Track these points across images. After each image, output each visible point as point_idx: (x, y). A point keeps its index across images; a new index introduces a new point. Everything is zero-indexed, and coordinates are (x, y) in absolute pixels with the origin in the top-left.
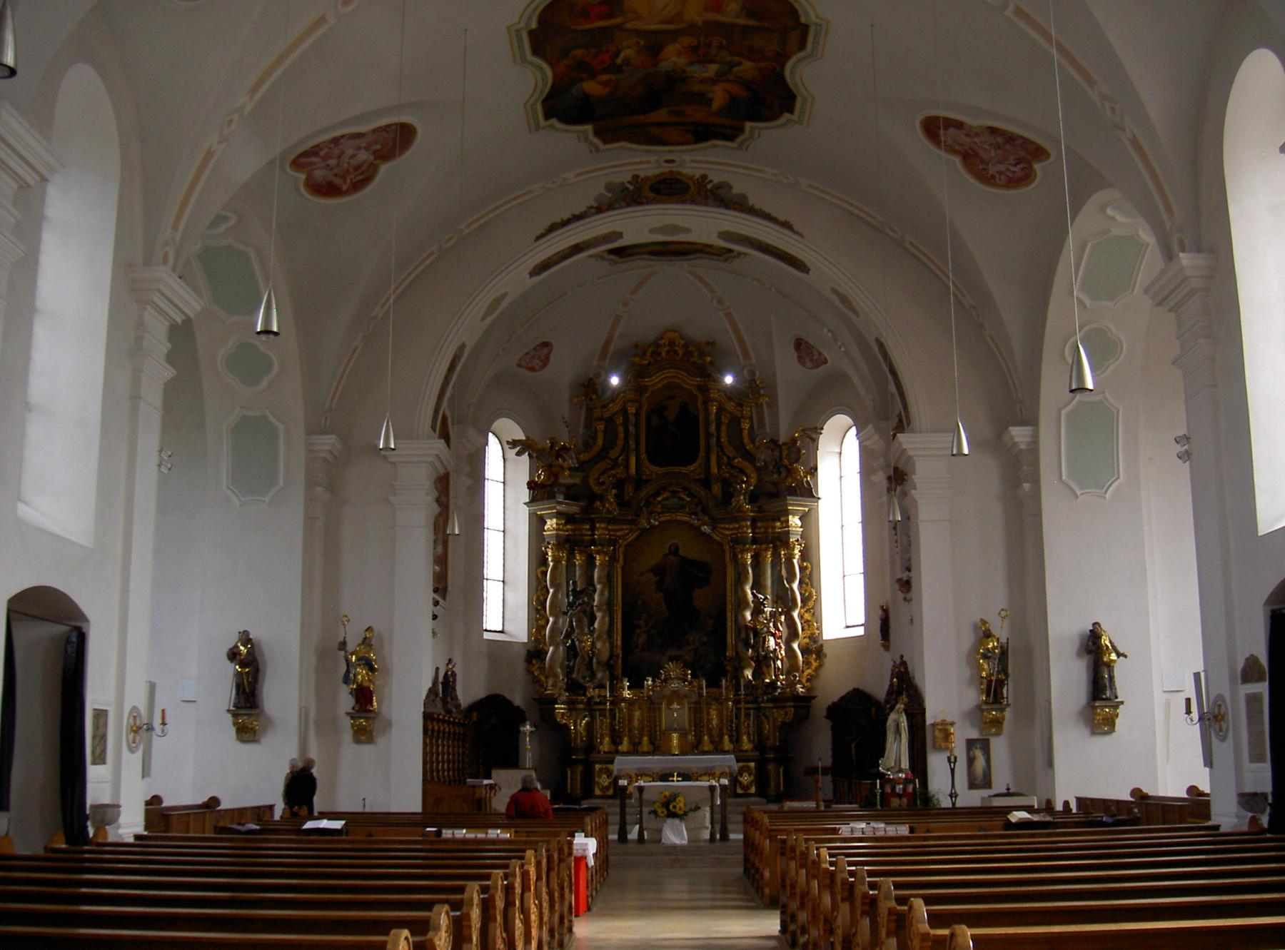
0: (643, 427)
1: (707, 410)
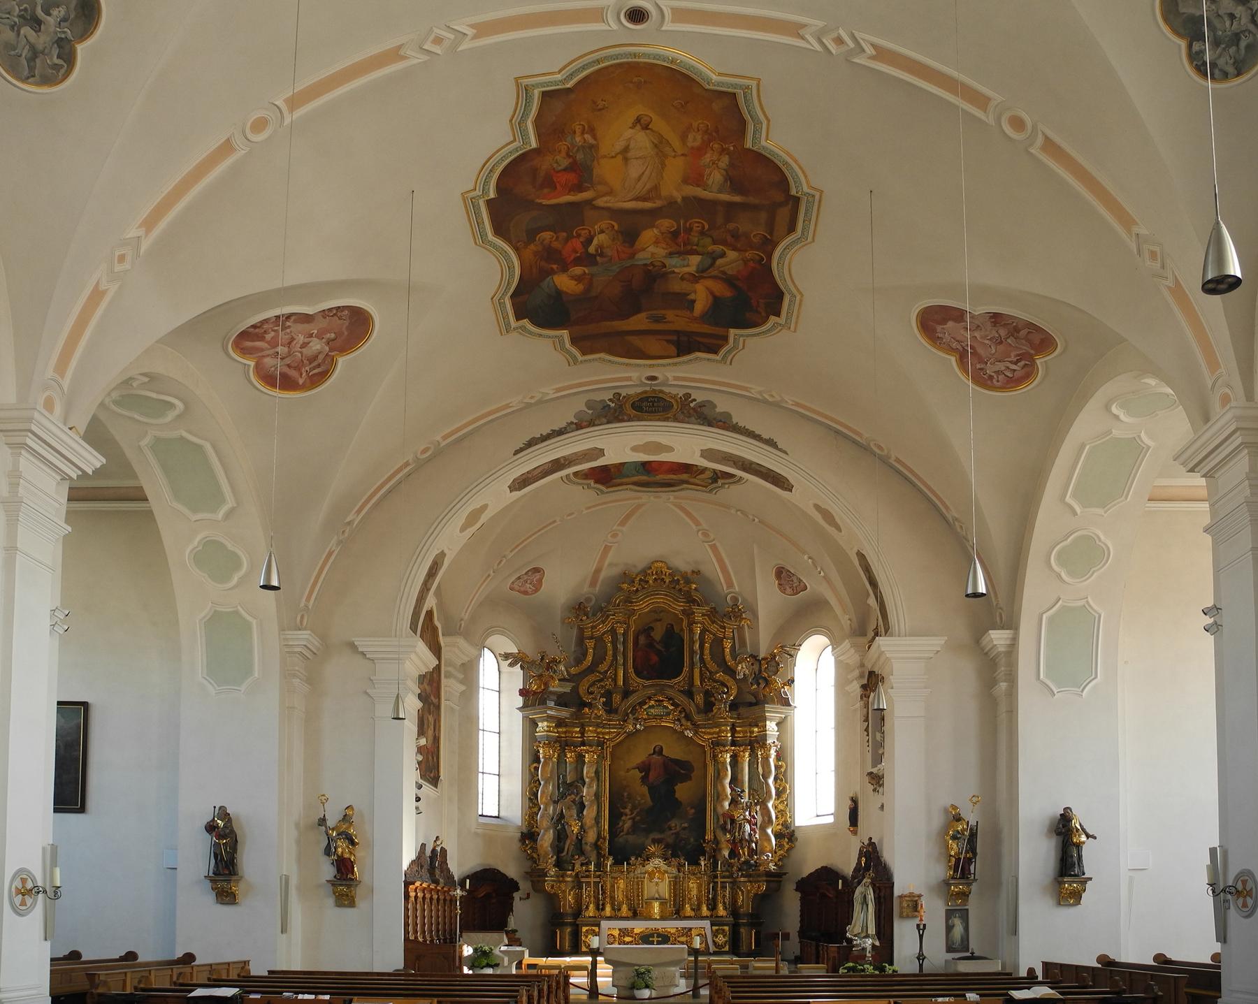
0: (631, 645)
1: (691, 631)
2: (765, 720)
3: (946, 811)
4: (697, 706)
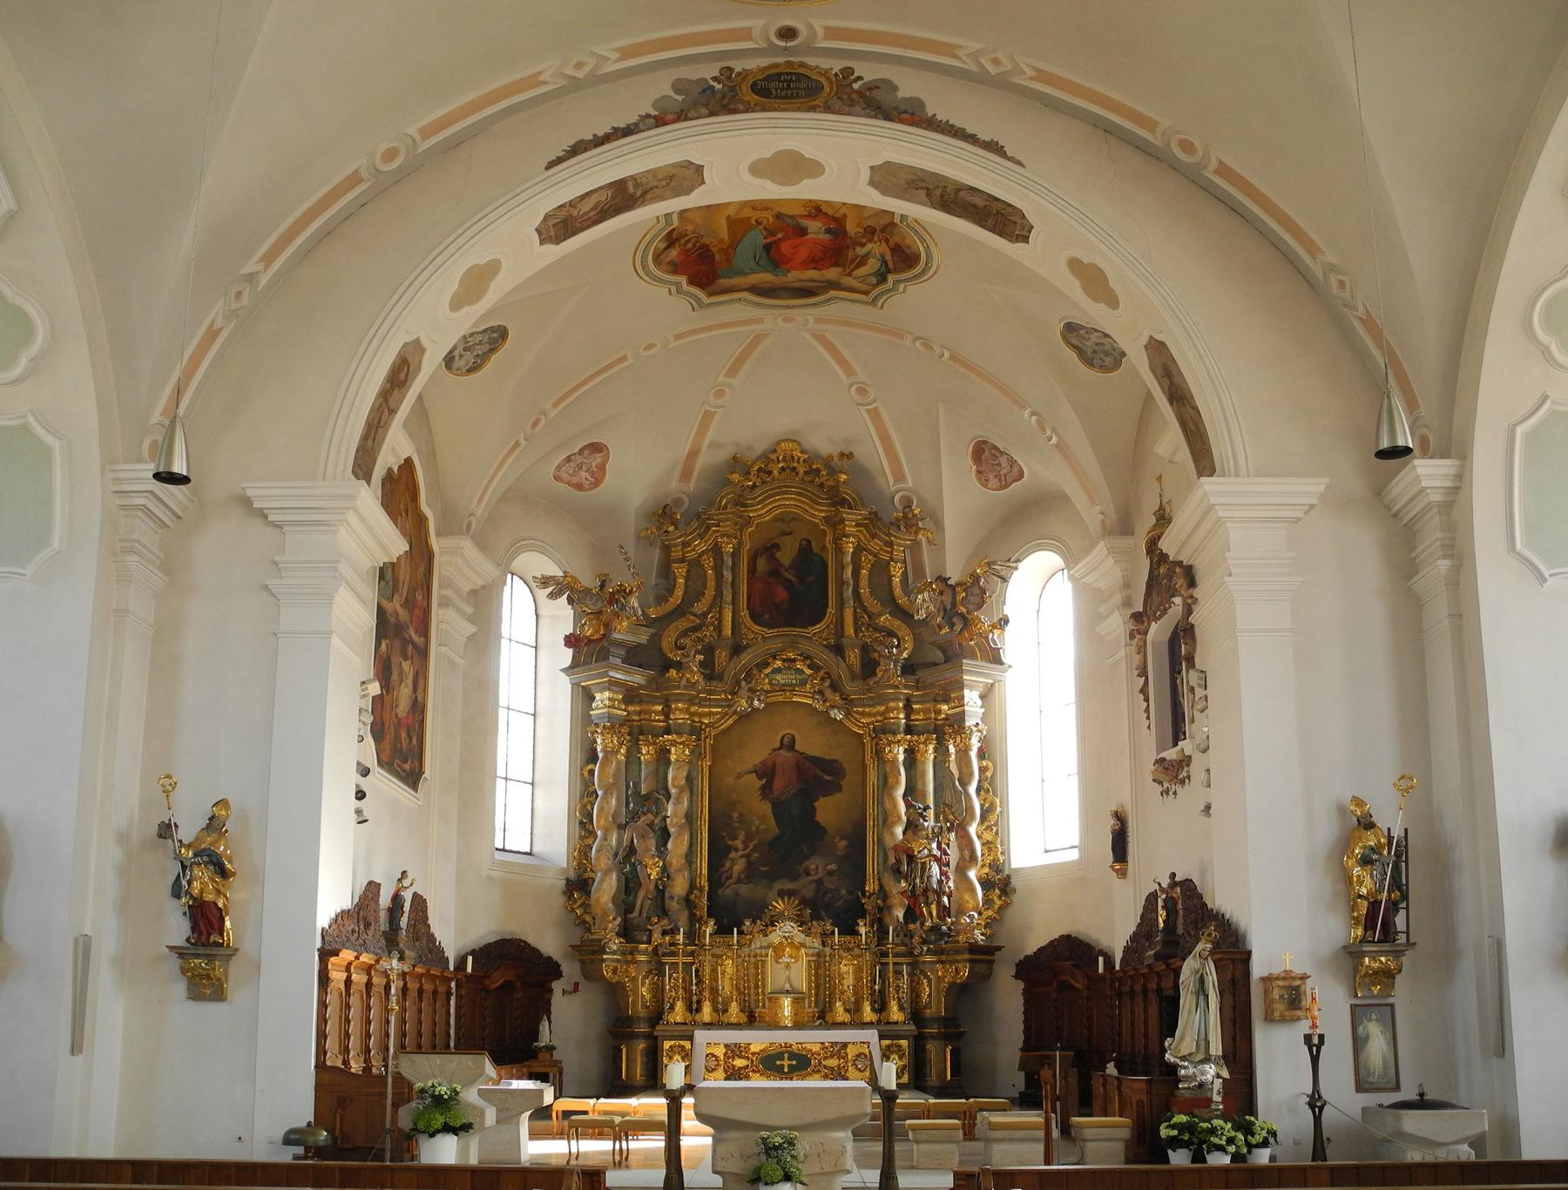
1: (839, 550)
2: (961, 688)
3: (1342, 811)
4: (850, 668)
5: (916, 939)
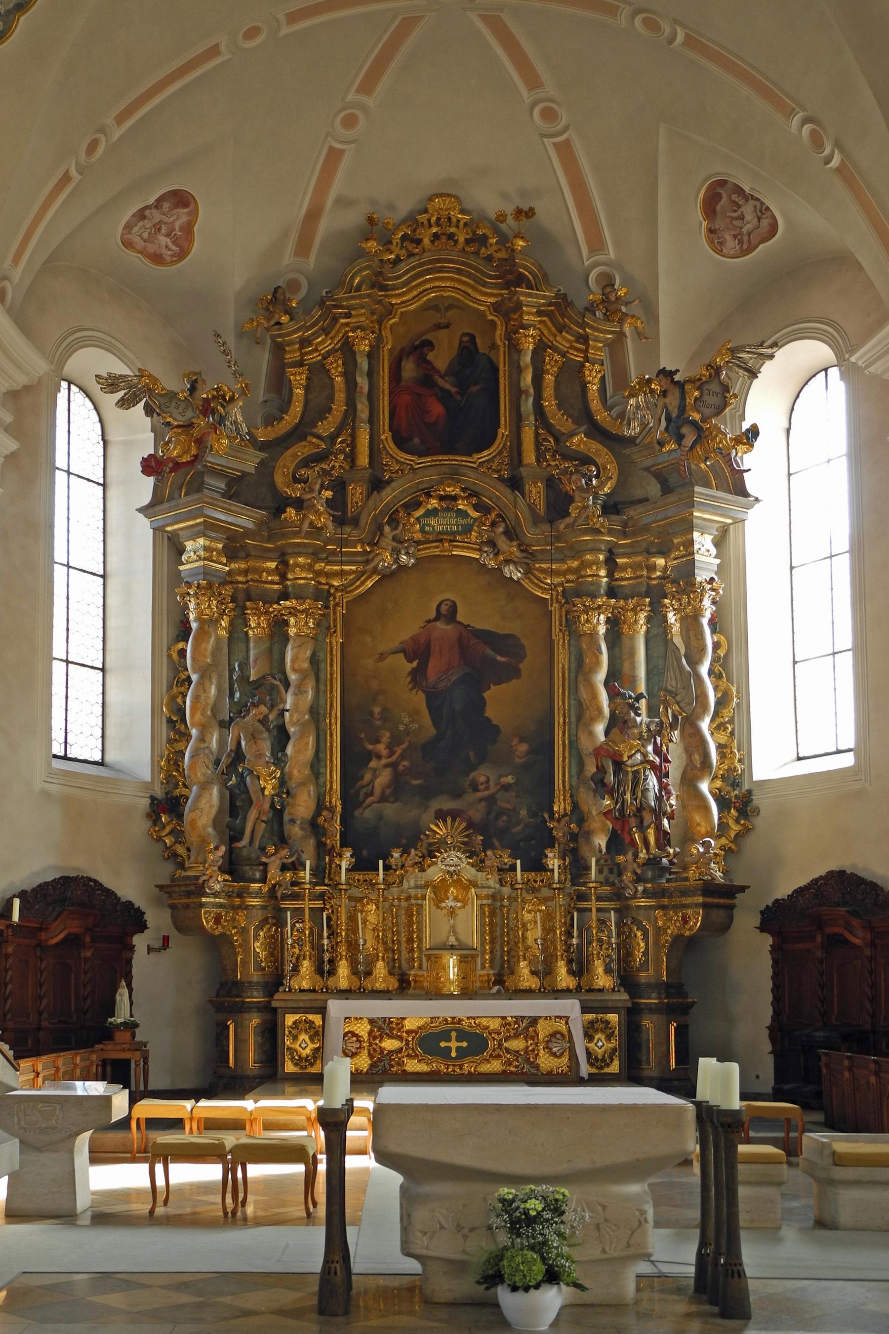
1: (514, 348)
2: (690, 529)
4: (532, 508)
5: (628, 877)
